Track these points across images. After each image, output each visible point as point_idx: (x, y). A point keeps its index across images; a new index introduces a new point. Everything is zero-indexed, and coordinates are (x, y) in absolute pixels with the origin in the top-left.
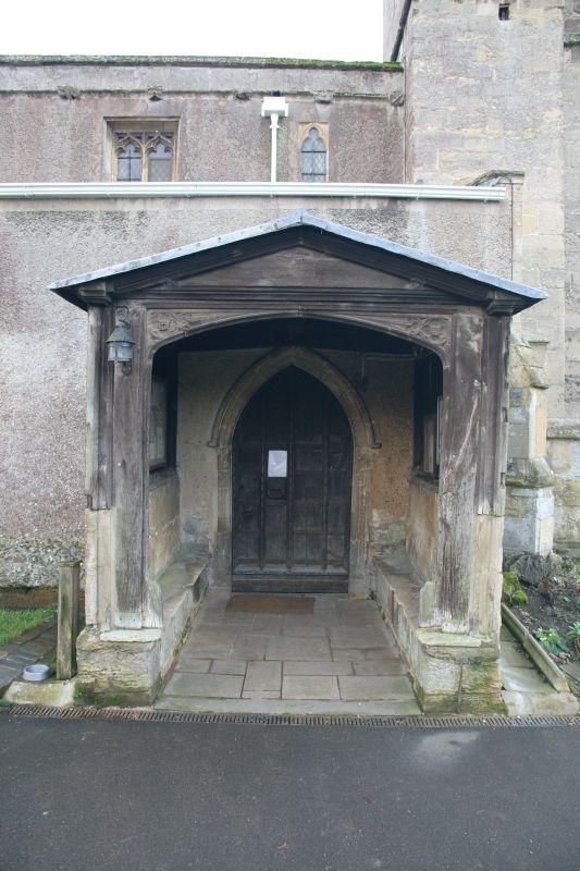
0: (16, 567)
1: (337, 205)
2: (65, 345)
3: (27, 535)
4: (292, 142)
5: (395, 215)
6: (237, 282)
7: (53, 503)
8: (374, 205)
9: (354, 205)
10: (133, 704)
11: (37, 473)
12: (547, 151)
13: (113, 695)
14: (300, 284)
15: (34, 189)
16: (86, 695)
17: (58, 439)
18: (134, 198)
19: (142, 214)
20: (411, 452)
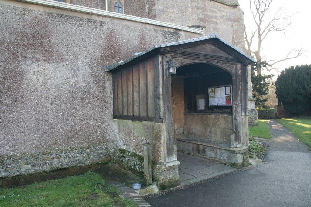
0: (57, 161)
1: (162, 29)
2: (73, 69)
3: (60, 147)
4: (112, 2)
5: (177, 34)
6: (195, 52)
7: (70, 132)
8: (172, 30)
9: (167, 30)
10: (176, 186)
11: (62, 121)
12: (189, 20)
13: (170, 185)
14: (210, 54)
15: (60, 4)
16: (162, 187)
17: (71, 106)
18: (99, 15)
19: (102, 22)
20: (184, 106)
